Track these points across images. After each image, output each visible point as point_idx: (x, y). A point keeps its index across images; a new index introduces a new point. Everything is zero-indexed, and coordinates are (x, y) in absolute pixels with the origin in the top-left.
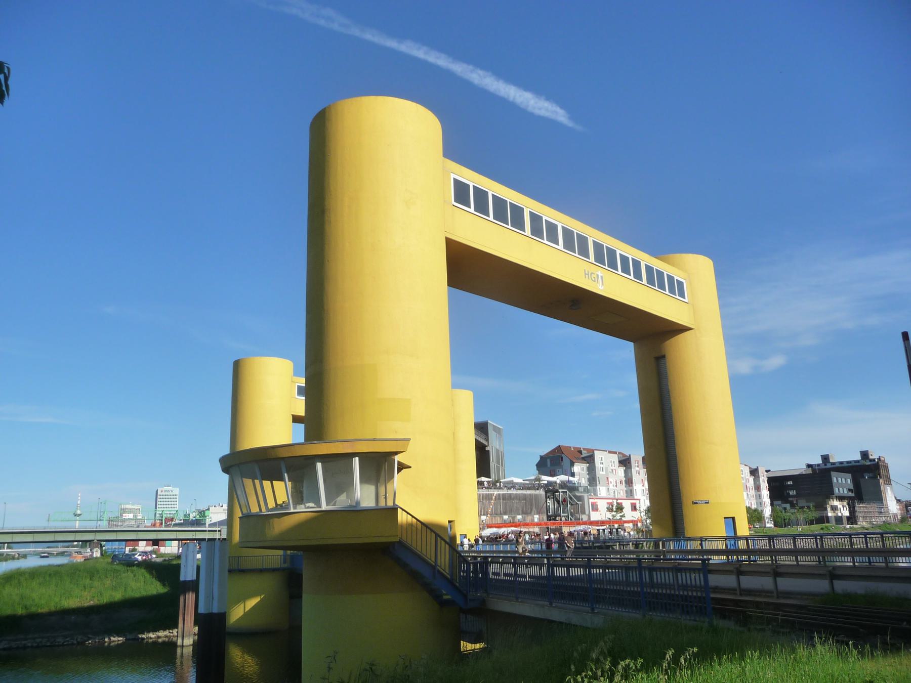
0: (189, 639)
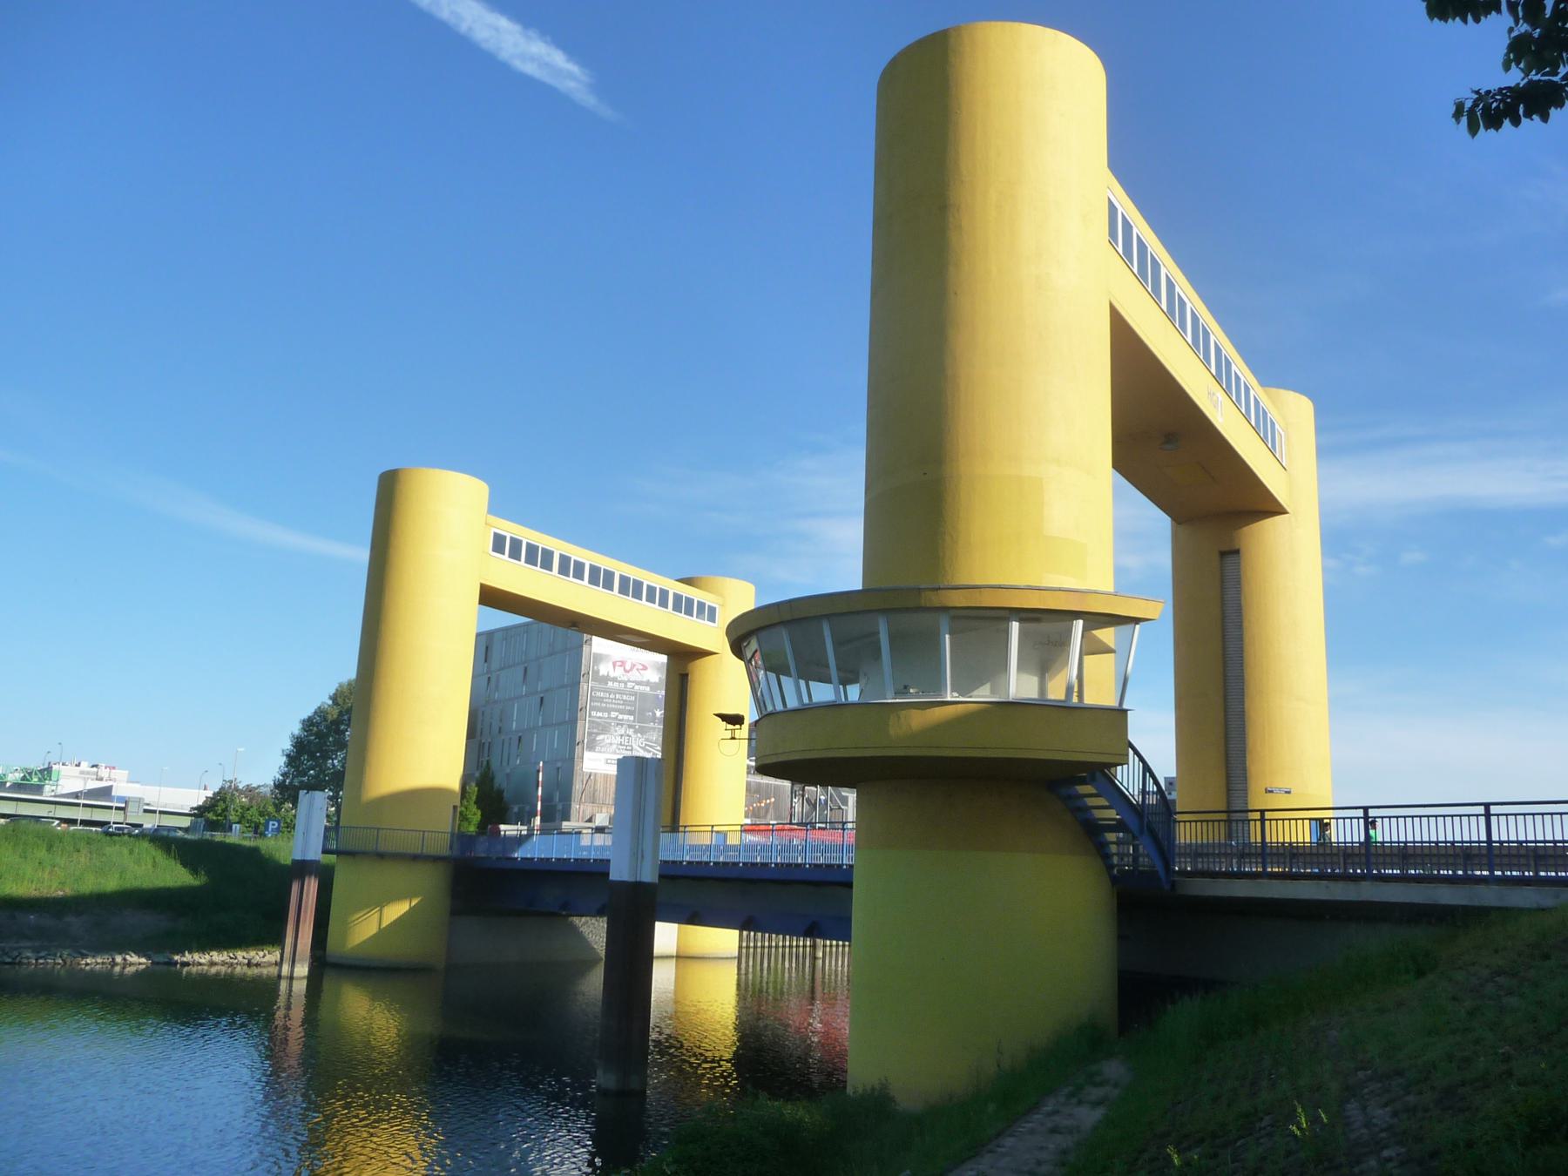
0: (303, 967)
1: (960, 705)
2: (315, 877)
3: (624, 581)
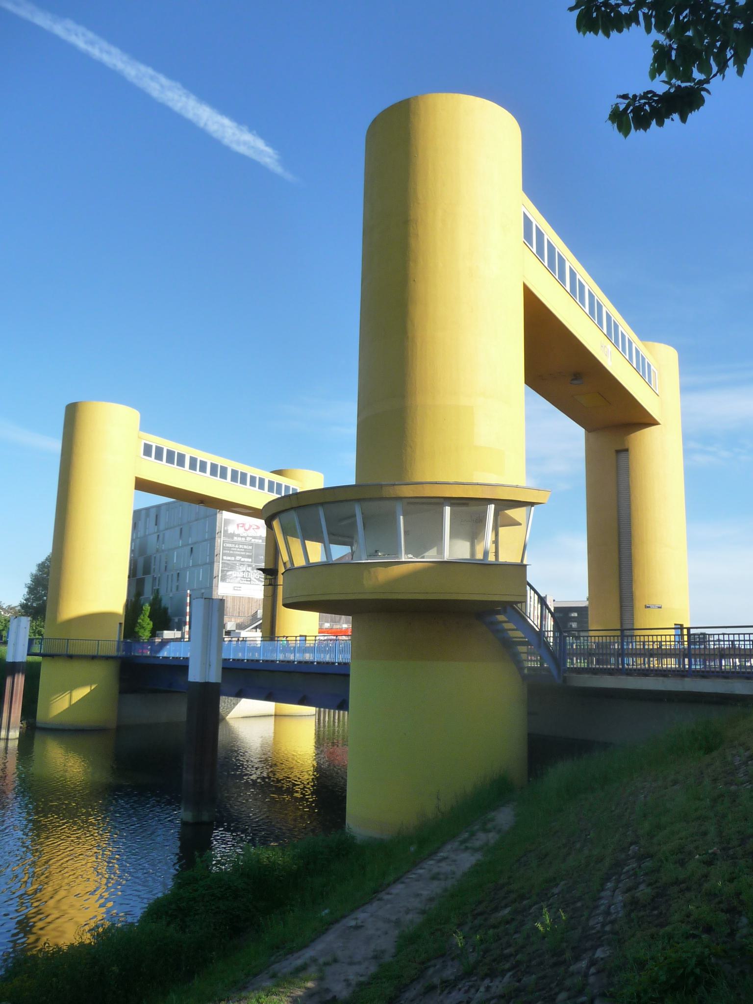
0: (15, 732)
1: (417, 564)
2: (22, 673)
3: (234, 473)
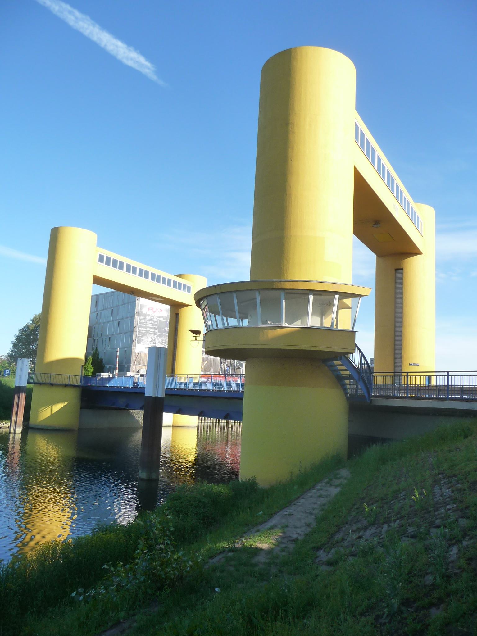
0: (19, 429)
2: (25, 393)
